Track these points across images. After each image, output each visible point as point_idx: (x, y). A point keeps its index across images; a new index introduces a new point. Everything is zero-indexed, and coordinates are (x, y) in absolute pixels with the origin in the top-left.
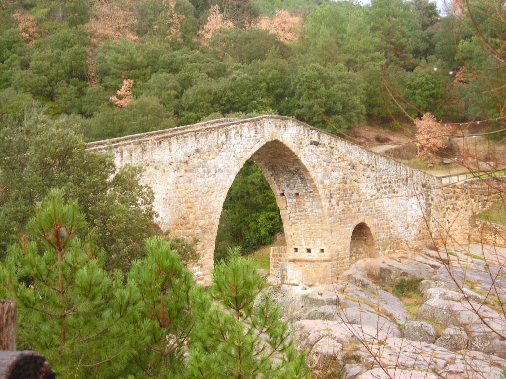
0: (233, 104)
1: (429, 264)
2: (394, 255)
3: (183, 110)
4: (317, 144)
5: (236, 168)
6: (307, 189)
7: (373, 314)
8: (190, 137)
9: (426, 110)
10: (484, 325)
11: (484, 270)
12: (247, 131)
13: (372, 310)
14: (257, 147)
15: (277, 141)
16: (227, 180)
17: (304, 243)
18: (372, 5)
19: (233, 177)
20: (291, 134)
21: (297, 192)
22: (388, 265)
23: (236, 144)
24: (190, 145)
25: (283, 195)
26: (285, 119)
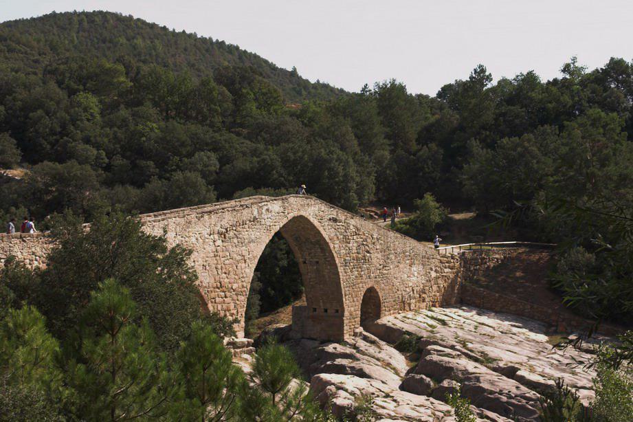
0: (263, 181)
1: (427, 324)
2: (398, 316)
3: (228, 187)
4: (335, 220)
5: (266, 239)
6: (325, 258)
7: (379, 367)
8: (227, 213)
9: (427, 191)
10: (581, 390)
11: (474, 330)
12: (276, 206)
13: (379, 363)
14: (285, 221)
15: (301, 217)
16: (258, 250)
17: (321, 304)
18: (493, 90)
19: (263, 248)
20: (314, 210)
21: (317, 260)
22: (393, 324)
23: (271, 214)
24: (228, 219)
25: (305, 262)
26: (309, 198)
